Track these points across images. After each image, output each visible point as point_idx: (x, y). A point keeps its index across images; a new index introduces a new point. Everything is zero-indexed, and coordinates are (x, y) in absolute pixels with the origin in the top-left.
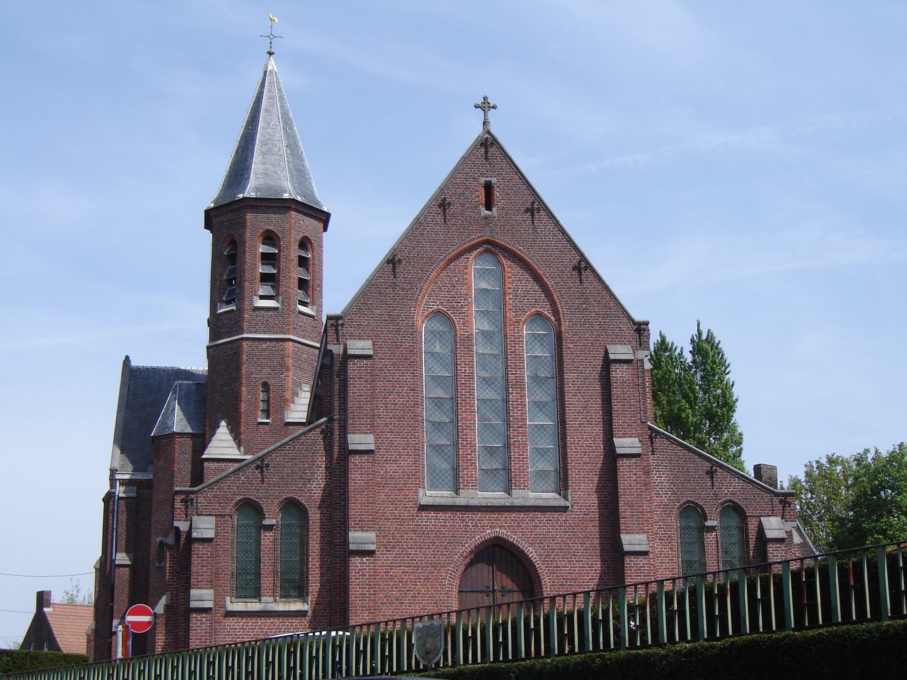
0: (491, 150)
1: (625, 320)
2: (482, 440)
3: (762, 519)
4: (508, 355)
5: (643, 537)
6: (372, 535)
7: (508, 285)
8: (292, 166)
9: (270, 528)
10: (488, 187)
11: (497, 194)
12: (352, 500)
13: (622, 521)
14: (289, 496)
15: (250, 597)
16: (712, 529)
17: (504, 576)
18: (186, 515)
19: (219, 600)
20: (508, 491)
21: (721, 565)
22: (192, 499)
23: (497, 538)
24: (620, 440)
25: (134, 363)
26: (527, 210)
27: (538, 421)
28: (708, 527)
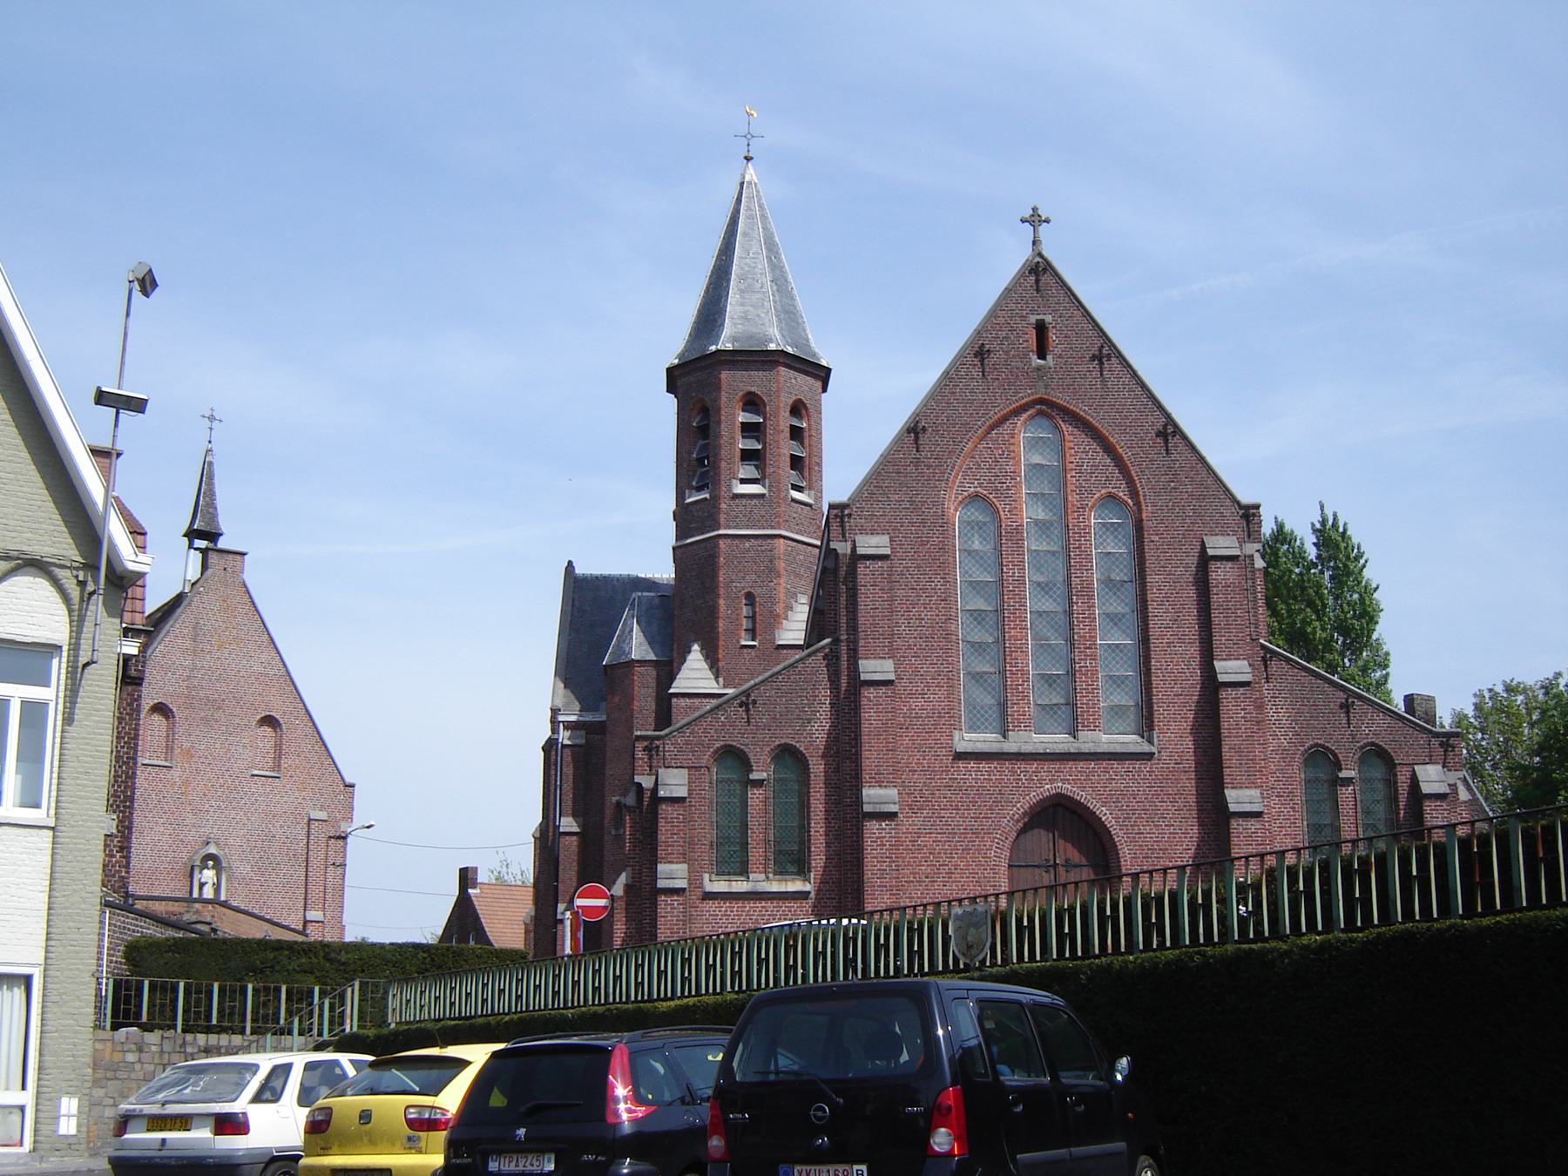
1: (1228, 503)
4: (1070, 553)
5: (1255, 793)
6: (892, 793)
10: (1041, 328)
11: (1052, 336)
12: (865, 747)
13: (1227, 771)
14: (788, 741)
16: (1349, 781)
17: (1069, 846)
19: (695, 880)
20: (1073, 733)
23: (1059, 795)
24: (1223, 663)
26: (1093, 358)
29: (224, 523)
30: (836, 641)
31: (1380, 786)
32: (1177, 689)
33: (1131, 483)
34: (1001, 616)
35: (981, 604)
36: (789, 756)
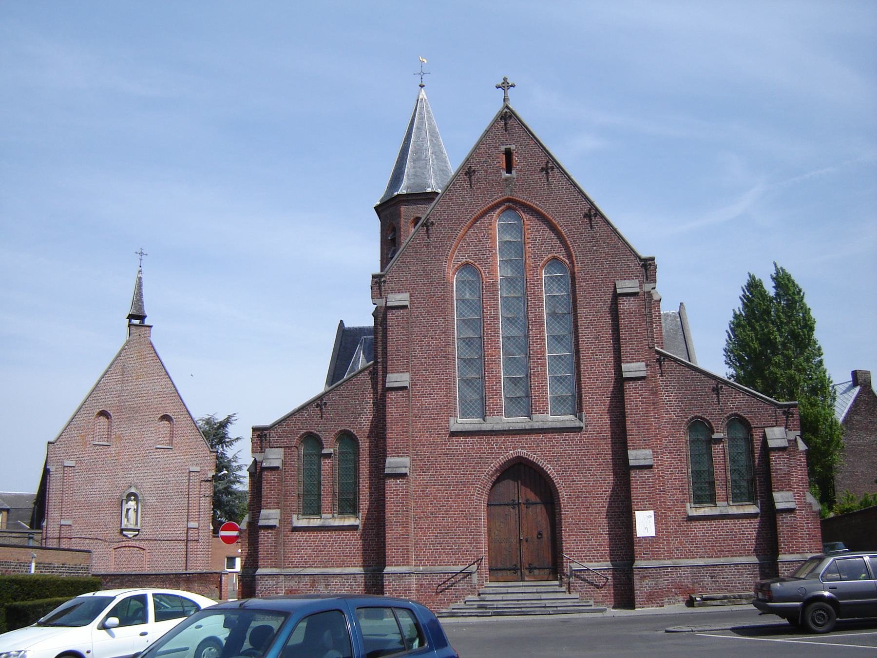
0: (510, 122)
1: (632, 257)
2: (507, 372)
3: (766, 429)
4: (526, 296)
5: (649, 452)
6: (406, 460)
7: (527, 236)
8: (435, 167)
9: (328, 456)
10: (508, 154)
11: (515, 158)
12: (389, 430)
13: (629, 438)
14: (343, 428)
15: (314, 514)
16: (719, 441)
17: (529, 490)
18: (261, 448)
19: (285, 520)
20: (529, 415)
21: (729, 474)
22: (266, 435)
23: (519, 457)
24: (628, 365)
25: (347, 325)
26: (542, 169)
27: (551, 352)
28: (715, 439)
29: (147, 311)
30: (376, 363)
31: (742, 443)
32: (599, 384)
33: (567, 248)
34: (479, 343)
35: (471, 334)
36: (347, 438)
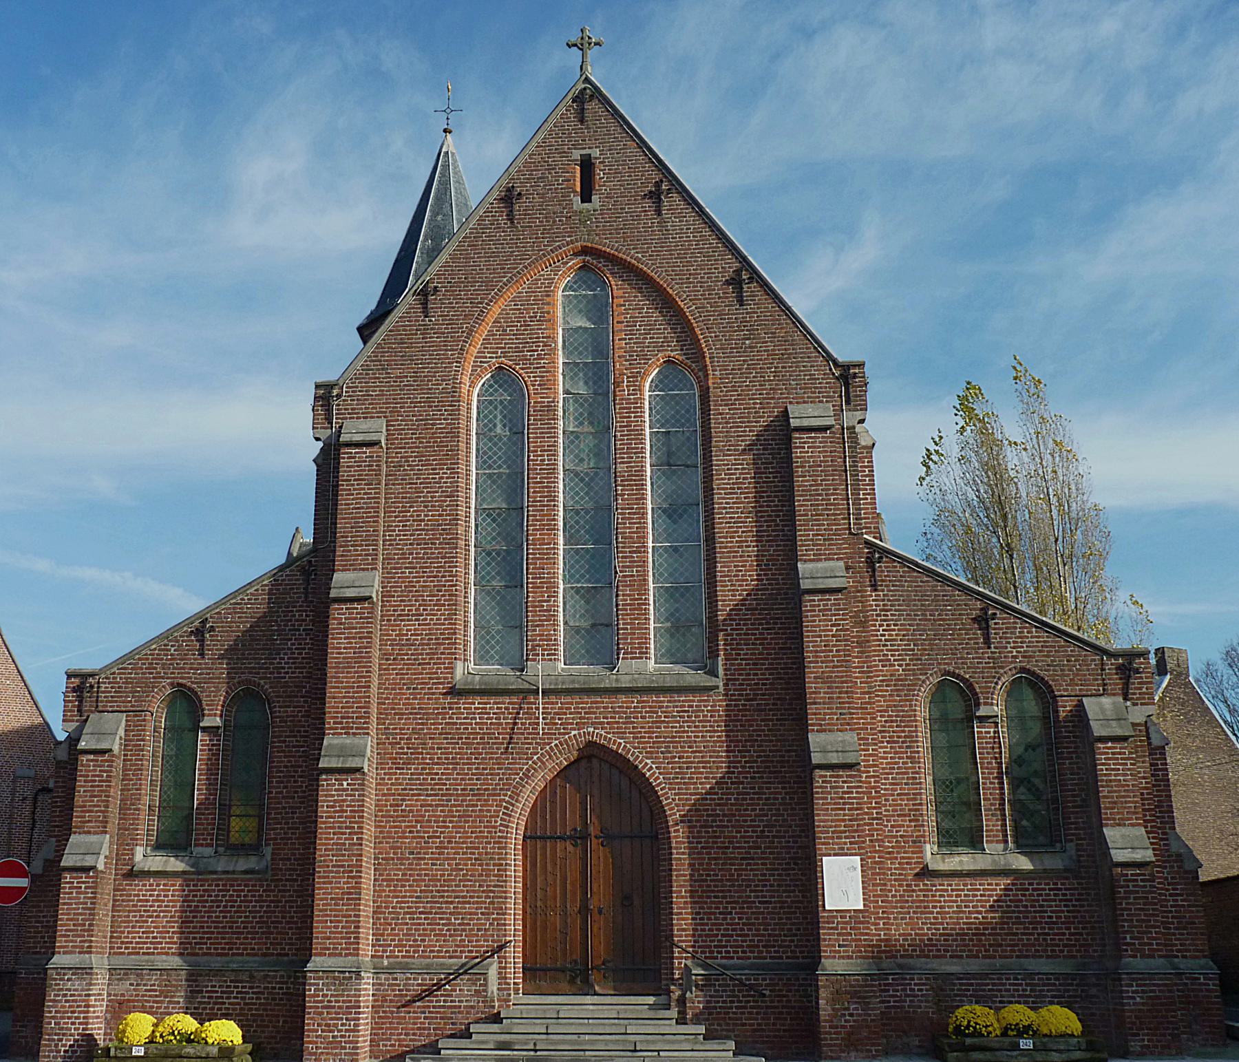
1: (797, 337)
2: (572, 576)
5: (851, 737)
10: (587, 165)
11: (599, 174)
12: (331, 683)
13: (811, 709)
24: (810, 565)
